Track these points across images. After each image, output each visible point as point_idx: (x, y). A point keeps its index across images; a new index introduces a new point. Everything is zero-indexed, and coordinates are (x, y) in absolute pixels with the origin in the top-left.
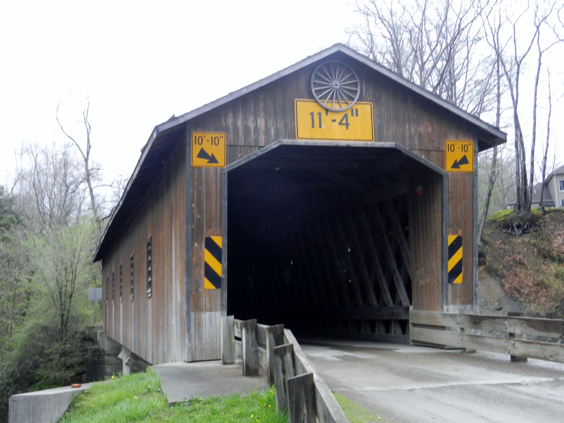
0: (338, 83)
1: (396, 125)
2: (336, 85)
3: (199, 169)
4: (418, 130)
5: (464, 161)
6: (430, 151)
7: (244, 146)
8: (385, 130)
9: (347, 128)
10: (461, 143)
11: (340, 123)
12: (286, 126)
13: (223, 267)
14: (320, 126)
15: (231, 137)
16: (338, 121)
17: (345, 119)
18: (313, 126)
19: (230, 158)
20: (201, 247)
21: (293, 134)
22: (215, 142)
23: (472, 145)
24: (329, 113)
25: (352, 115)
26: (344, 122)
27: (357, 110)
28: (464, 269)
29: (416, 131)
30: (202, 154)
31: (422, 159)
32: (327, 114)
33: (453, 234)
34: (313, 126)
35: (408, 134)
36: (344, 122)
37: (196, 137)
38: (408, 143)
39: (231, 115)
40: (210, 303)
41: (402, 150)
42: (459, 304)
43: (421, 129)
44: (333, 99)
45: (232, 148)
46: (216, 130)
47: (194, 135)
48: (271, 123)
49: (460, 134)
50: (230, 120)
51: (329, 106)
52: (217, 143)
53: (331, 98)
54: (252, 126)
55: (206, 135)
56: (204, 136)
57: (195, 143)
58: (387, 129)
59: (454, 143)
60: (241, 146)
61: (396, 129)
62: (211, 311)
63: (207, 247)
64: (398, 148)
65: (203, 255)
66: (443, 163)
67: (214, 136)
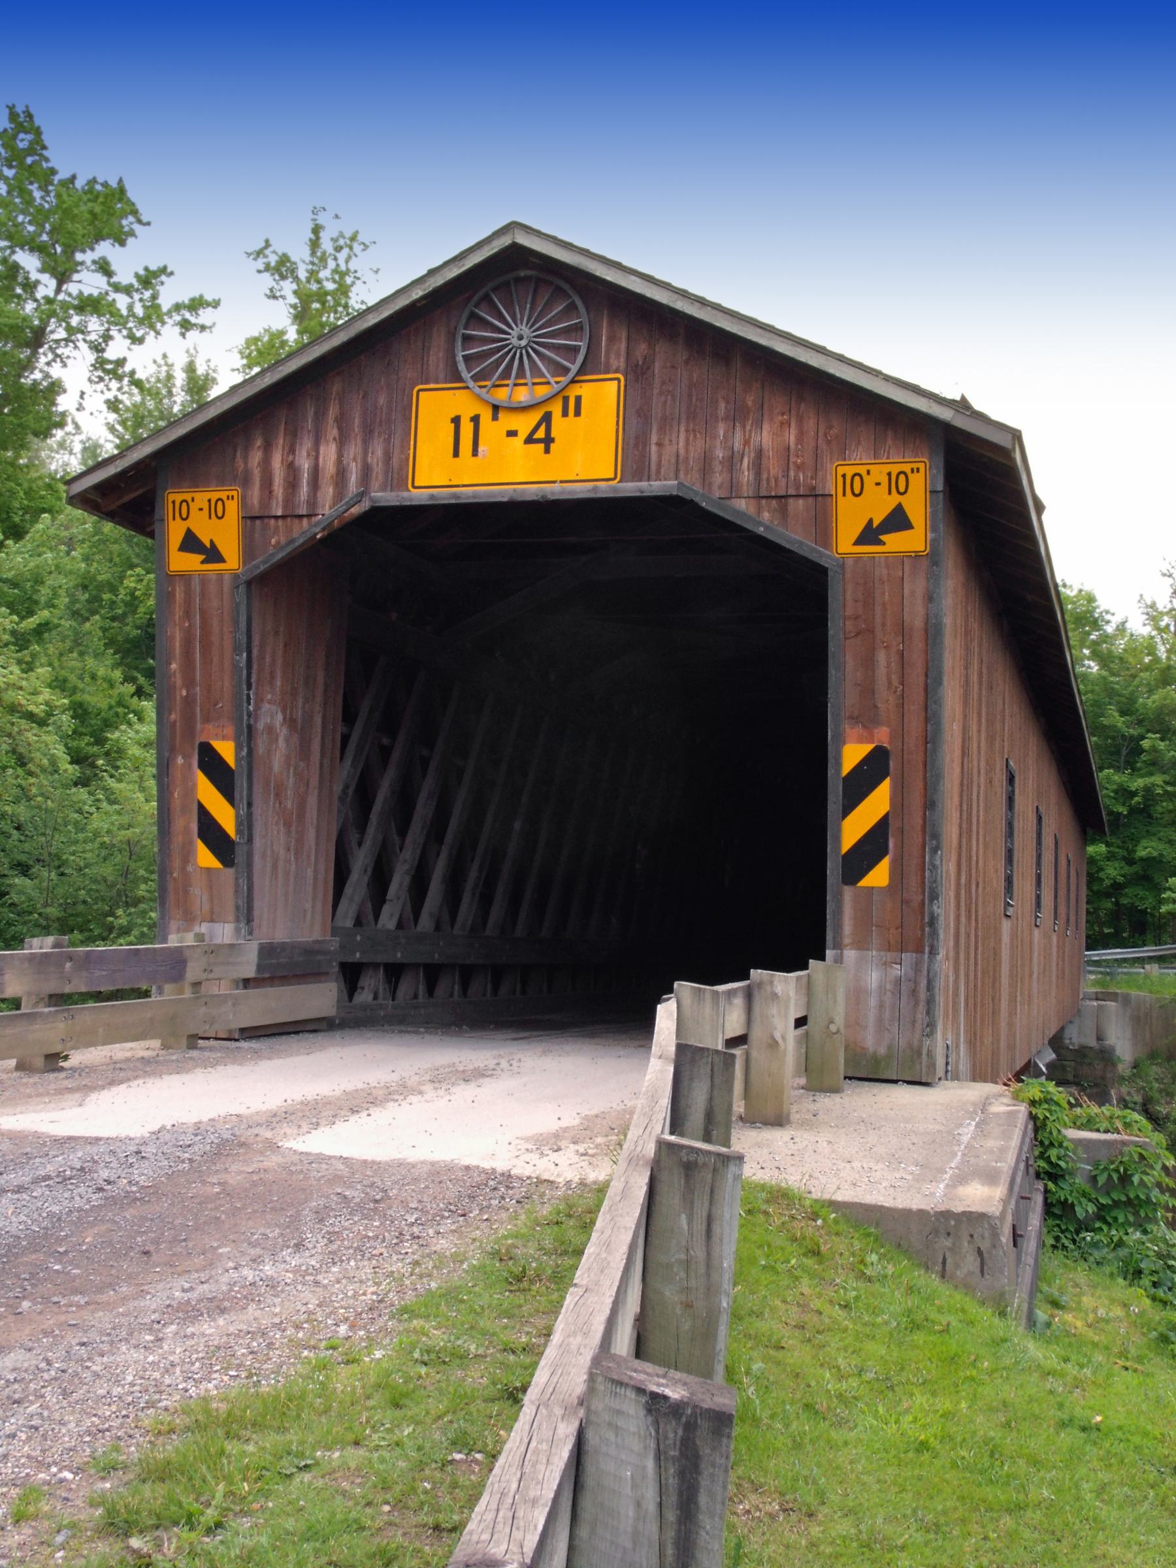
0: (515, 333)
1: (687, 431)
2: (520, 338)
3: (185, 578)
4: (755, 440)
5: (898, 520)
6: (786, 497)
7: (283, 517)
8: (654, 448)
9: (547, 451)
10: (888, 468)
11: (529, 440)
12: (388, 457)
13: (237, 816)
14: (475, 453)
15: (255, 493)
16: (523, 435)
17: (543, 429)
18: (456, 454)
19: (248, 550)
20: (190, 766)
21: (399, 476)
22: (216, 511)
23: (922, 470)
24: (501, 415)
25: (565, 414)
26: (541, 434)
27: (578, 399)
28: (895, 847)
29: (747, 443)
30: (191, 543)
31: (760, 524)
32: (495, 418)
33: (860, 741)
34: (456, 454)
35: (720, 454)
36: (541, 434)
37: (174, 502)
38: (719, 478)
39: (259, 442)
40: (211, 900)
41: (697, 499)
42: (878, 950)
43: (766, 437)
44: (524, 377)
45: (258, 522)
46: (222, 481)
47: (171, 497)
48: (353, 450)
49: (890, 442)
50: (256, 457)
51: (502, 395)
52: (220, 514)
53: (521, 373)
54: (305, 465)
55: (197, 496)
56: (193, 500)
57: (844, 495)
58: (659, 444)
59: (862, 470)
60: (276, 517)
61: (687, 439)
62: (212, 921)
63: (203, 767)
64: (688, 496)
65: (195, 786)
66: (823, 527)
67: (214, 496)
